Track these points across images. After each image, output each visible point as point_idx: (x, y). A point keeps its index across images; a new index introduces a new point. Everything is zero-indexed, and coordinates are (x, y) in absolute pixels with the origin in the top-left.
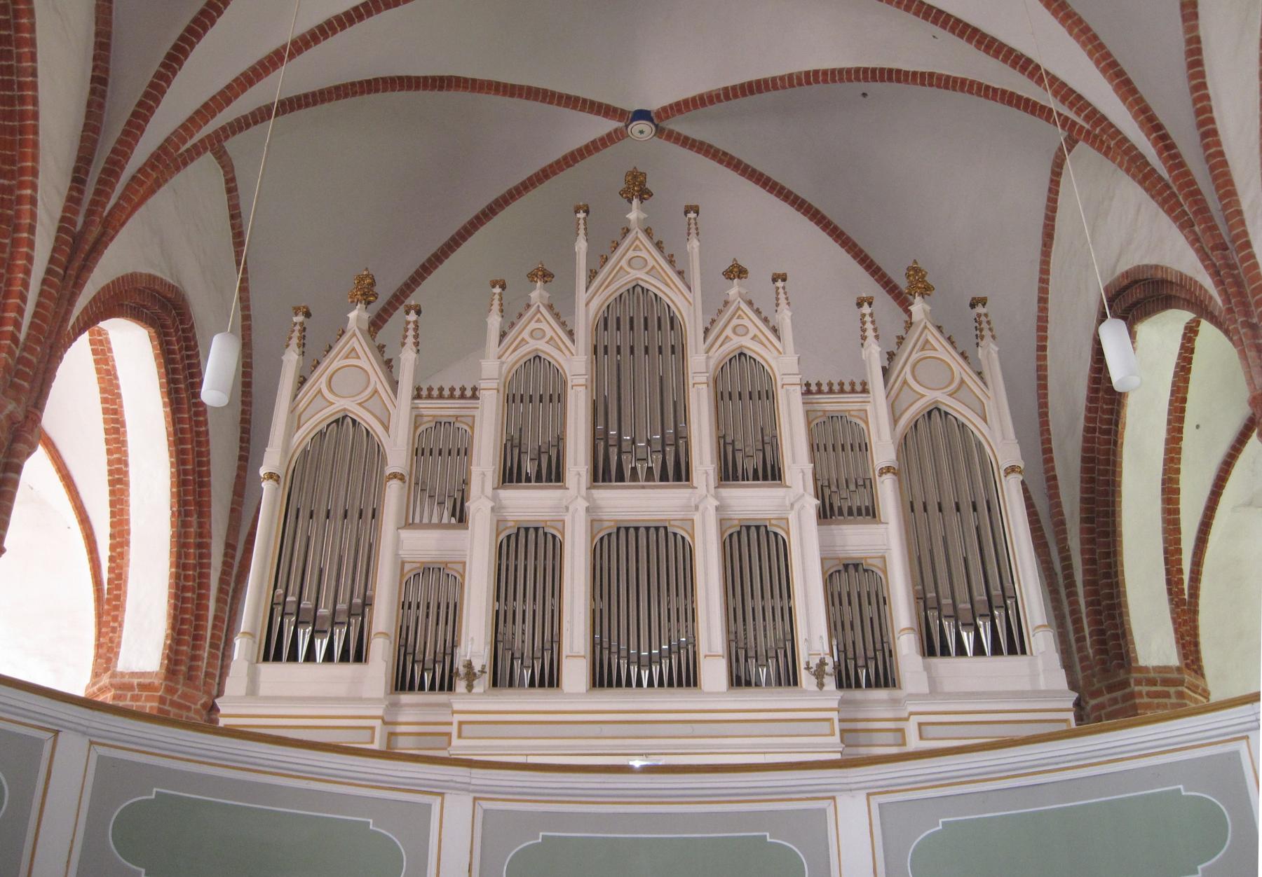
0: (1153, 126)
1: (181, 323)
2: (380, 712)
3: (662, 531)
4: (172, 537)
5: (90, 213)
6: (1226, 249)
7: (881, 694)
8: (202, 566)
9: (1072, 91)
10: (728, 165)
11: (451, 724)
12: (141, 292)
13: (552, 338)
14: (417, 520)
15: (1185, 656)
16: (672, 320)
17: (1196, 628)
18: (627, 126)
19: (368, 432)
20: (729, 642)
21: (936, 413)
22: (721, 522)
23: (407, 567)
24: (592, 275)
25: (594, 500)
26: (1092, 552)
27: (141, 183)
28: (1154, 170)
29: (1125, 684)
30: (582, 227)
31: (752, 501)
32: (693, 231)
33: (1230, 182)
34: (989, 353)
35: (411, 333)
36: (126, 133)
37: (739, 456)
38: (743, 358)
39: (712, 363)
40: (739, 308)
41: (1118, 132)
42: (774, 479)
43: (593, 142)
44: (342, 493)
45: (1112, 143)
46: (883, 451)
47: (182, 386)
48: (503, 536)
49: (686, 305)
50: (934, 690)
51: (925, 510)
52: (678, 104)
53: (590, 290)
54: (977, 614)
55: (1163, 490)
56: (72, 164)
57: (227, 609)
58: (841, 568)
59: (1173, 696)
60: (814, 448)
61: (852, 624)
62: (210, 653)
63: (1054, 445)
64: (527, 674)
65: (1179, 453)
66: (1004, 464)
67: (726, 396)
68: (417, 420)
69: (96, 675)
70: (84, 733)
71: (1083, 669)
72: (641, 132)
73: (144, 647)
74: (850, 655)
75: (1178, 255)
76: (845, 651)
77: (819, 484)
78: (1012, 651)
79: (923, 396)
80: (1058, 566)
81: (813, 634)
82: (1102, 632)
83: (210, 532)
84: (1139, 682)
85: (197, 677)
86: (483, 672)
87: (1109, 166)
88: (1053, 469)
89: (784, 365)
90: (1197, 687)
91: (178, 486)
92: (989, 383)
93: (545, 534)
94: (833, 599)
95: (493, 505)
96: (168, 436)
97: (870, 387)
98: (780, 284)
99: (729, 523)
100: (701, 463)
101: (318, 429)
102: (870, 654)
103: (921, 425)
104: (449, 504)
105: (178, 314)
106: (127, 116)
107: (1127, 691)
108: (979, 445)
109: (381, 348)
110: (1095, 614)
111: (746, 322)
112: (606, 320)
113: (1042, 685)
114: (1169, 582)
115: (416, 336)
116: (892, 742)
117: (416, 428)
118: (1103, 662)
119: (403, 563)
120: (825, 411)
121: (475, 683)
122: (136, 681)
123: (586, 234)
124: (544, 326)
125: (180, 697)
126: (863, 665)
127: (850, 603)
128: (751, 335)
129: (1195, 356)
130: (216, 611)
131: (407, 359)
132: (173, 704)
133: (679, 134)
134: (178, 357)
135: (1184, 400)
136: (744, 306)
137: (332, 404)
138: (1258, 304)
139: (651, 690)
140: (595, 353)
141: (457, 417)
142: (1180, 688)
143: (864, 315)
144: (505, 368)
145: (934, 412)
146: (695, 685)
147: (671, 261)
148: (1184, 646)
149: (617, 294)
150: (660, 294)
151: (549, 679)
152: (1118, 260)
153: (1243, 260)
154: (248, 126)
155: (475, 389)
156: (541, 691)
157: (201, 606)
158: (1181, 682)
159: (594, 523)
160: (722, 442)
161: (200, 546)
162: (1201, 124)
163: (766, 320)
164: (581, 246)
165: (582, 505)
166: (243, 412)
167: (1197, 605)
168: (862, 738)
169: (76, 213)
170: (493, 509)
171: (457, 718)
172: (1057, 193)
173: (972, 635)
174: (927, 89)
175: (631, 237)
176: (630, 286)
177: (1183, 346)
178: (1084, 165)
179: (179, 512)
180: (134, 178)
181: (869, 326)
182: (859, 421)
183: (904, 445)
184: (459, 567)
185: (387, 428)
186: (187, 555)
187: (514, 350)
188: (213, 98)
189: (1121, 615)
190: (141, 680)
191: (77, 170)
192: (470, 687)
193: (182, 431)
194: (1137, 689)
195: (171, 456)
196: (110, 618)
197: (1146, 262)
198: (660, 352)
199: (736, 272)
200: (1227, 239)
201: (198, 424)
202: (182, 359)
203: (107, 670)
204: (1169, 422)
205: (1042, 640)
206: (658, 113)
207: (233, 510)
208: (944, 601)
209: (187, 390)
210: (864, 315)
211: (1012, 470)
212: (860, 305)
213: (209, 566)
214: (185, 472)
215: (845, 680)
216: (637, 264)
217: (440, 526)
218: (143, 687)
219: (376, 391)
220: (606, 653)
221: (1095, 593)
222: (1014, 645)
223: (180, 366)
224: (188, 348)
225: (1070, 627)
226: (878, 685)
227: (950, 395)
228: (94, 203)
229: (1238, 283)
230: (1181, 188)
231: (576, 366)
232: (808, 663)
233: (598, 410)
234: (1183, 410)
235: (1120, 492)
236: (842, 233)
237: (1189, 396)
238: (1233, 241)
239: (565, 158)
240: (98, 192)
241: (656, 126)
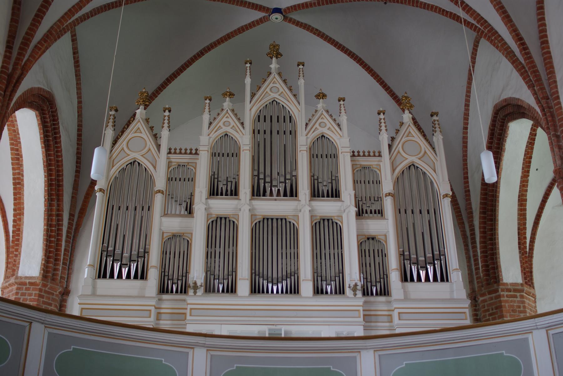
1: (51, 108)
2: (154, 303)
3: (284, 221)
4: (45, 211)
5: (16, 64)
6: (548, 99)
7: (382, 299)
8: (59, 225)
9: (482, 18)
10: (318, 35)
11: (186, 309)
12: (34, 95)
13: (233, 126)
14: (169, 212)
15: (525, 278)
16: (290, 117)
17: (531, 265)
18: (270, 16)
19: (146, 169)
20: (314, 273)
21: (412, 167)
22: (312, 217)
23: (165, 235)
24: (253, 95)
25: (253, 205)
26: (484, 228)
27: (40, 49)
28: (518, 59)
29: (497, 291)
30: (248, 71)
31: (326, 208)
32: (301, 75)
33: (552, 67)
34: (438, 139)
35: (166, 121)
36: (32, 24)
37: (320, 185)
38: (323, 138)
39: (309, 140)
40: (322, 114)
41: (503, 39)
42: (336, 197)
43: (253, 22)
44: (126, 192)
45: (500, 45)
46: (387, 186)
47: (51, 138)
48: (210, 221)
49: (298, 111)
50: (406, 298)
51: (406, 213)
52: (295, 6)
53: (252, 103)
54: (427, 262)
55: (519, 200)
56: (6, 39)
57: (70, 246)
58: (366, 239)
59: (519, 297)
60: (355, 182)
61: (370, 264)
62: (62, 267)
63: (469, 175)
64: (221, 287)
65: (527, 182)
66: (443, 192)
67: (315, 156)
69: (6, 277)
70: (42, 323)
71: (478, 282)
72: (277, 19)
73: (31, 264)
74: (369, 280)
75: (527, 97)
76: (367, 279)
77: (357, 199)
78: (442, 280)
79: (407, 159)
80: (468, 233)
81: (352, 273)
83: (63, 209)
84: (503, 290)
85: (57, 279)
86: (201, 286)
87: (497, 52)
88: (468, 187)
89: (343, 143)
90: (530, 293)
91: (48, 187)
92: (438, 154)
93: (230, 221)
94: (362, 253)
95: (206, 207)
96: (44, 163)
97: (382, 154)
98: (342, 102)
99: (314, 218)
100: (303, 189)
101: (122, 167)
102: (378, 280)
103: (405, 172)
104: (184, 205)
105: (50, 104)
106: (33, 16)
107: (497, 294)
108: (432, 183)
109: (152, 128)
110: (484, 257)
111: (325, 121)
112: (259, 116)
113: (455, 296)
114: (519, 243)
115: (169, 123)
116: (386, 321)
117: (169, 168)
118: (487, 280)
119: (163, 233)
120: (361, 165)
121: (198, 290)
122: (27, 281)
123: (250, 75)
124: (229, 120)
125: (49, 288)
126: (375, 285)
127: (369, 256)
128: (327, 127)
129: (537, 137)
130: (65, 246)
131: (165, 134)
132: (46, 292)
133: (295, 20)
134: (49, 124)
135: (531, 158)
136: (325, 113)
137: (129, 155)
138: (560, 126)
139: (277, 295)
140: (254, 133)
141: (188, 163)
142: (522, 294)
143: (381, 119)
144: (211, 140)
145: (412, 166)
146: (298, 293)
147: (290, 90)
148: (525, 274)
149: (264, 105)
150: (285, 105)
151: (231, 289)
152: (502, 93)
153: (555, 105)
154: (88, 18)
155: (196, 150)
156: (227, 295)
157: (58, 245)
158: (522, 291)
159: (252, 216)
160: (313, 178)
161: (58, 215)
162: (541, 37)
163: (335, 120)
164: (248, 81)
165: (246, 208)
166: (78, 149)
167: (532, 253)
168: (373, 318)
169: (9, 64)
170: (205, 209)
171: (189, 307)
172: (476, 55)
173: (424, 272)
174: (415, 8)
175: (271, 77)
176: (271, 101)
177: (531, 134)
178: (486, 49)
179: (48, 199)
180: (36, 46)
181: (383, 124)
182: (376, 170)
183: (397, 182)
184: (189, 236)
185: (155, 168)
186: (52, 220)
187: (216, 132)
188: (73, 7)
189: (496, 258)
190: (31, 281)
191: (8, 42)
192: (195, 293)
193: (50, 160)
194: (502, 293)
195: (45, 172)
196: (14, 250)
197: (514, 96)
198: (285, 134)
199: (321, 96)
200: (549, 94)
201: (58, 156)
202: (51, 126)
203: (13, 275)
204: (523, 168)
205: (457, 277)
206: (285, 10)
207: (73, 197)
208: (412, 256)
209: (53, 140)
210: (381, 119)
211: (446, 196)
212: (379, 114)
213: (62, 225)
214: (51, 180)
215: (366, 292)
216: (274, 90)
217: (180, 216)
218: (31, 284)
219: (150, 150)
220: (257, 277)
221: (485, 247)
222: (444, 278)
223: (50, 129)
224: (54, 120)
225: (472, 259)
226: (381, 295)
227: (419, 159)
228: (17, 59)
229: (552, 116)
230: (529, 68)
231: (245, 140)
232: (350, 285)
233: (255, 161)
234: (530, 162)
235: (498, 201)
236: (372, 70)
237: (533, 156)
238: (552, 95)
239: (239, 29)
240: (19, 54)
241: (284, 16)
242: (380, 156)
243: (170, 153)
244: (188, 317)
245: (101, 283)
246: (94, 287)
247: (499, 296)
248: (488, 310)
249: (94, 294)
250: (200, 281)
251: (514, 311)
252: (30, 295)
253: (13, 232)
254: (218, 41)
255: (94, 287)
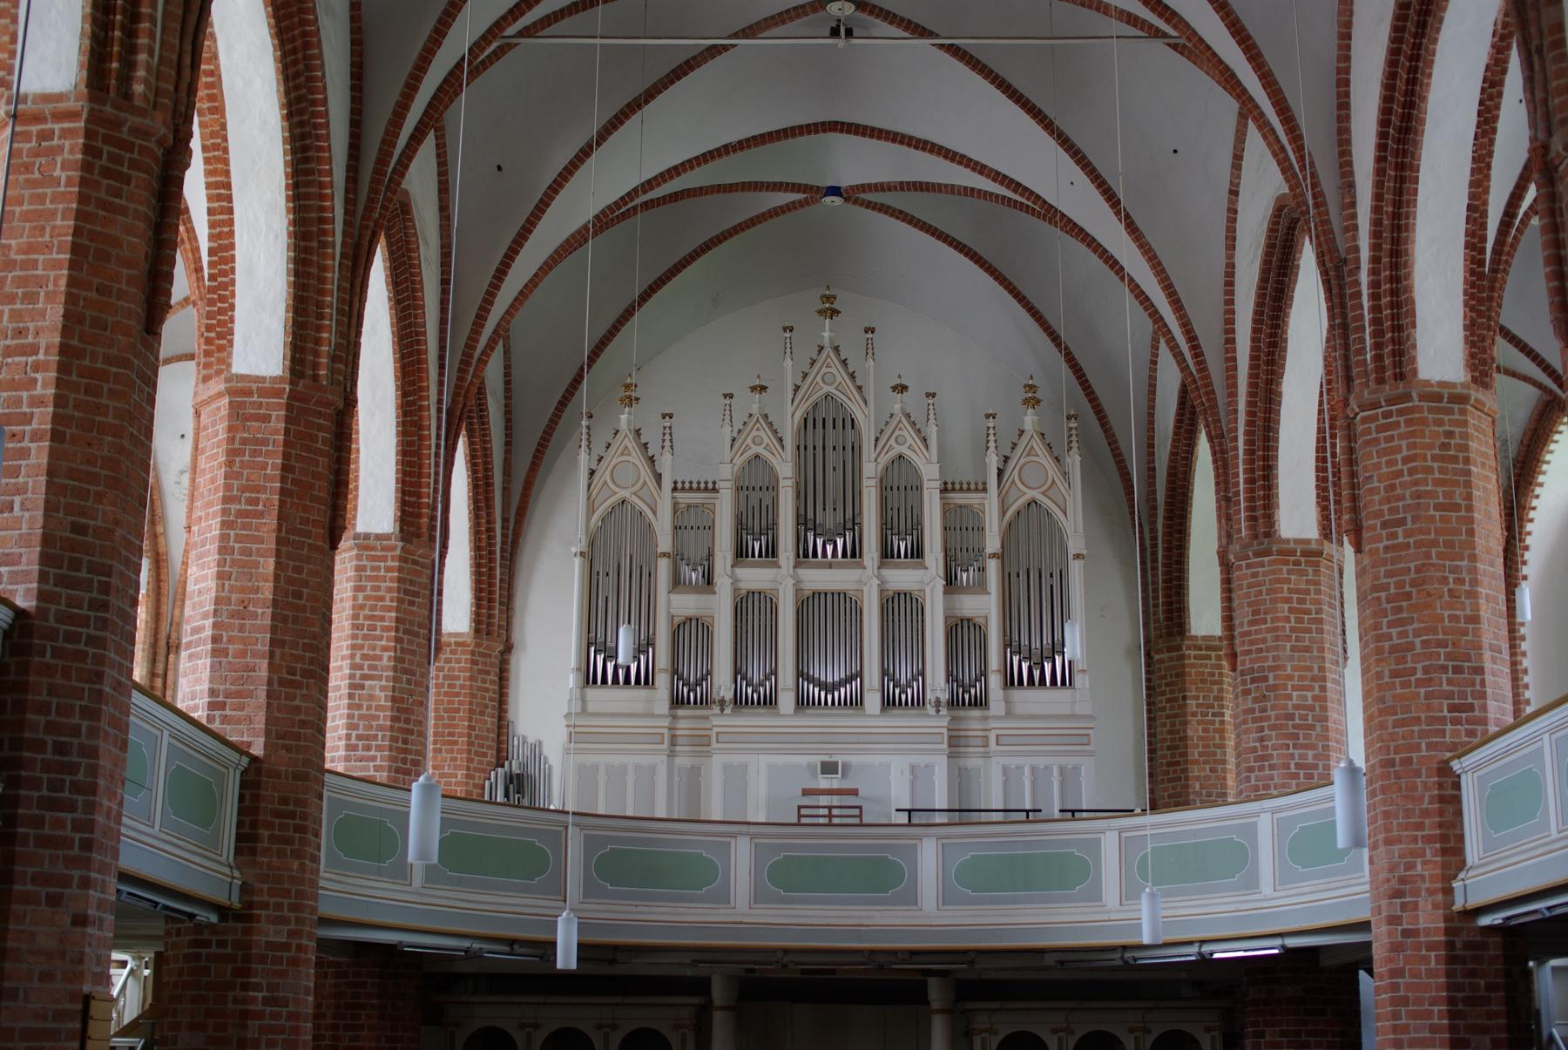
0: (1192, 338)
10: (903, 220)
29: (1179, 648)
31: (902, 578)
39: (880, 467)
50: (1009, 714)
68: (675, 505)
81: (937, 683)
82: (1170, 604)
84: (1188, 648)
103: (1022, 514)
111: (905, 433)
126: (966, 697)
132: (481, 655)
145: (1033, 503)
159: (798, 591)
168: (963, 741)
181: (992, 438)
192: (722, 710)
218: (458, 644)
231: (785, 469)
233: (801, 495)
242: (985, 490)
243: (675, 489)
244: (715, 745)
245: (592, 693)
246: (583, 700)
247: (1182, 657)
248: (1165, 677)
249: (584, 711)
250: (729, 696)
251: (1203, 681)
252: (458, 661)
253: (211, 252)
254: (734, 228)
255: (583, 700)
